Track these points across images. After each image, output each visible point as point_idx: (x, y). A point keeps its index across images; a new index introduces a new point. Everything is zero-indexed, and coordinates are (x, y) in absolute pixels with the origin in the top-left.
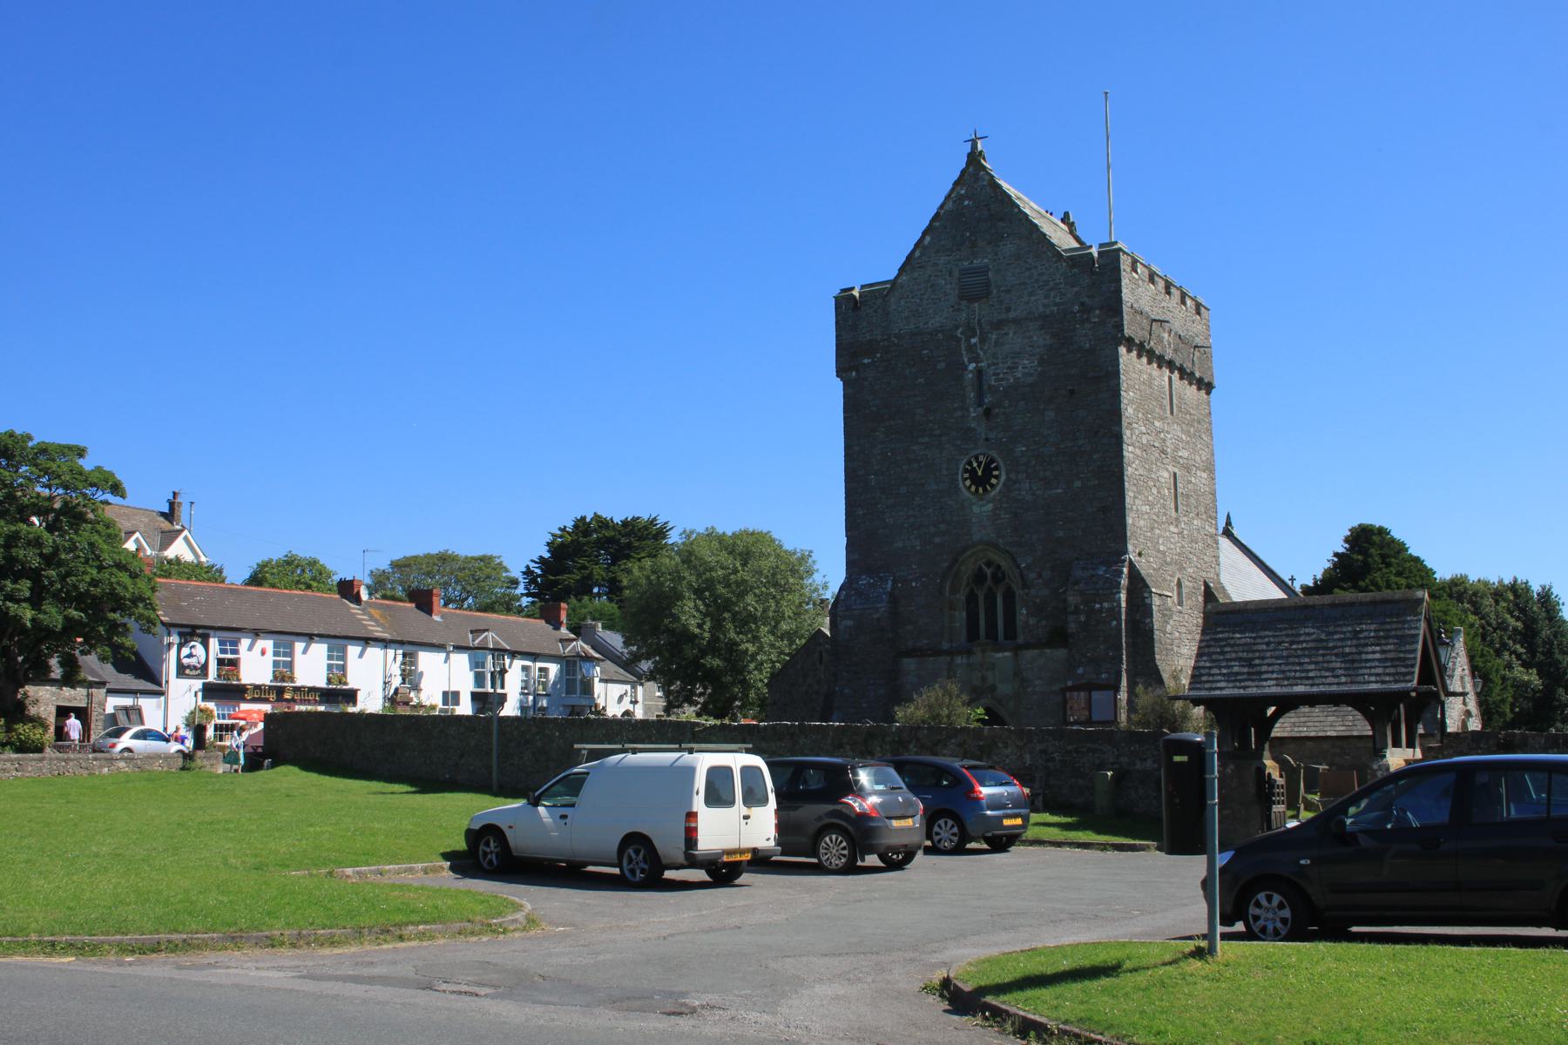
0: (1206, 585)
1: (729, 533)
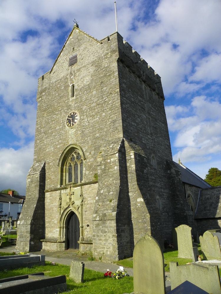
0: (167, 162)
1: (117, 245)
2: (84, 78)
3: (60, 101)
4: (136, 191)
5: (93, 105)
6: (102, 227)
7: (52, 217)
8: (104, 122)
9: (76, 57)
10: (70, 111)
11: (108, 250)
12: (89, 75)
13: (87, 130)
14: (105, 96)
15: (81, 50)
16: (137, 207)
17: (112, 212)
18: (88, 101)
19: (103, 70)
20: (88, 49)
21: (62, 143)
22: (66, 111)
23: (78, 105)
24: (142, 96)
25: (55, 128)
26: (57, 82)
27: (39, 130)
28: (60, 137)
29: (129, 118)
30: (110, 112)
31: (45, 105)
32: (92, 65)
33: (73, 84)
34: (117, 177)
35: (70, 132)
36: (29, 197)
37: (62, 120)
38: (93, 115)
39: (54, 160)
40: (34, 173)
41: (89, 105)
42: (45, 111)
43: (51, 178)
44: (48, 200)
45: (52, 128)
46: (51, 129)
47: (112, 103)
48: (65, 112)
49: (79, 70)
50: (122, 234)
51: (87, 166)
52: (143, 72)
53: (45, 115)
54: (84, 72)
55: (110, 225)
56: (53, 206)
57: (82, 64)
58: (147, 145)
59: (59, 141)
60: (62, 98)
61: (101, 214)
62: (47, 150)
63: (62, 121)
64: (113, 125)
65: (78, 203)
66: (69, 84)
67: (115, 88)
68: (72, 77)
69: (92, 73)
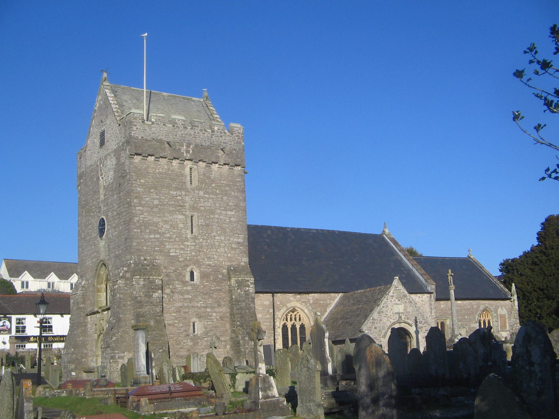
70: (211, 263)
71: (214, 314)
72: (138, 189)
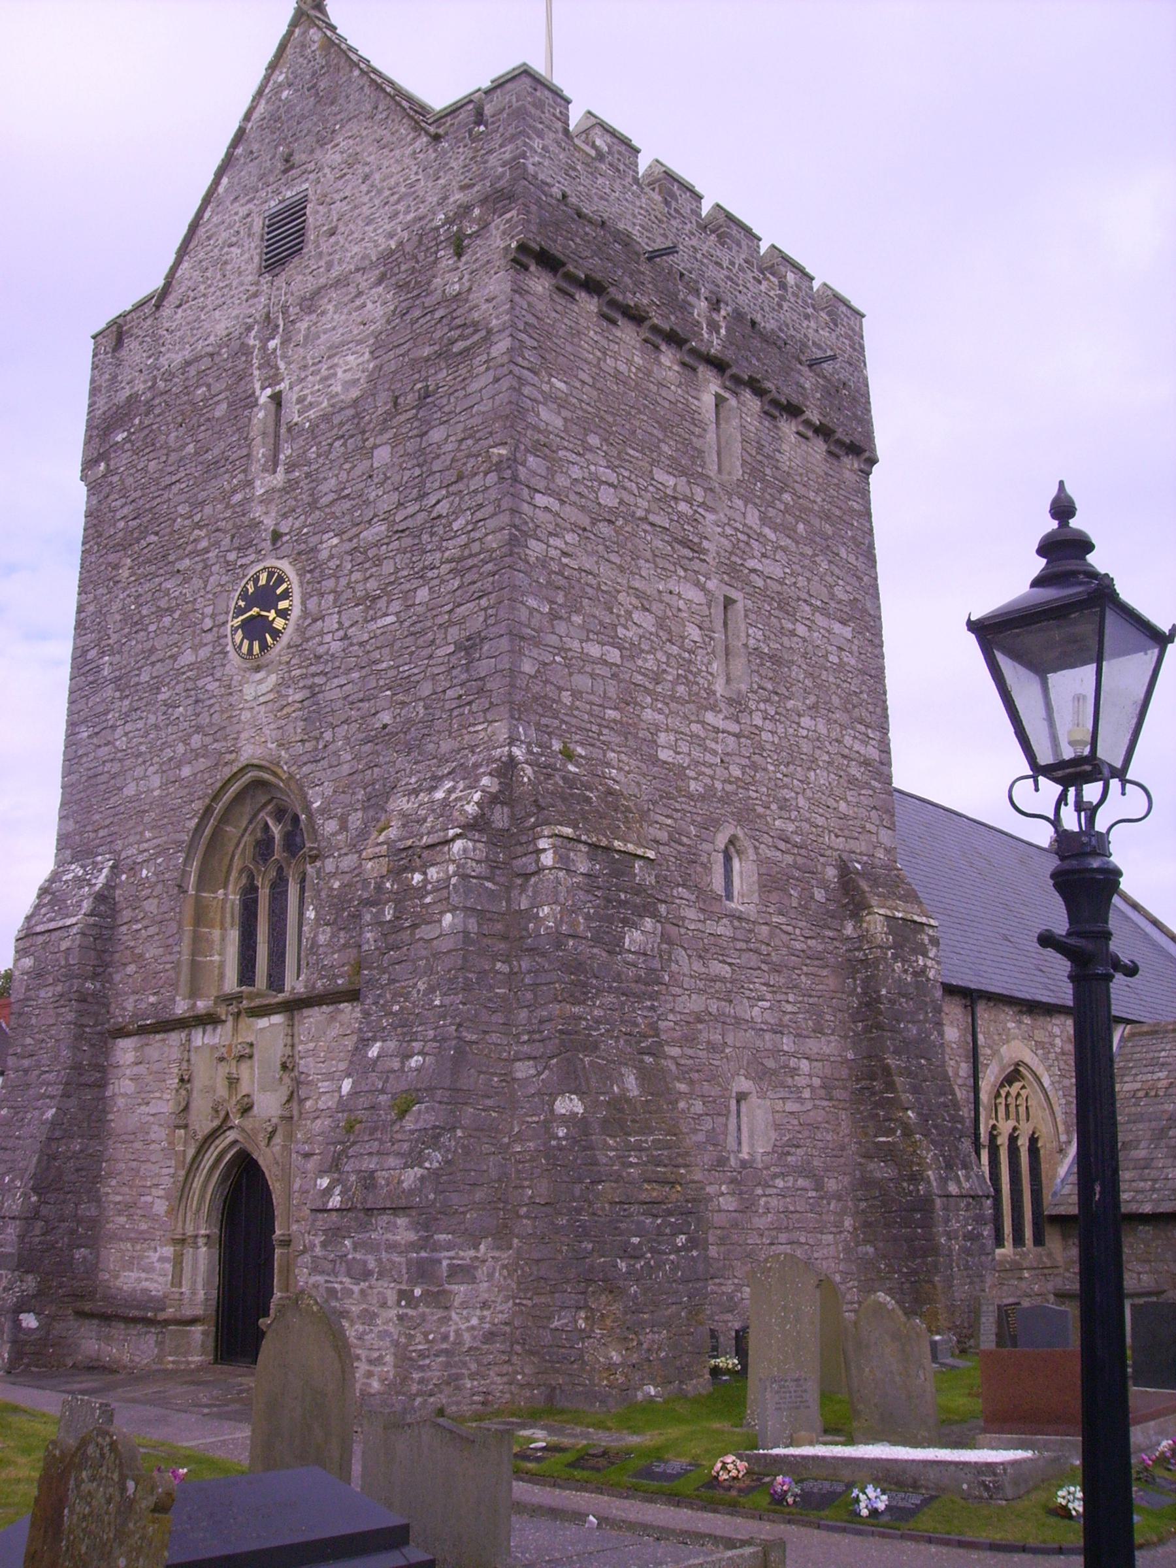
0: (844, 869)
2: (336, 360)
3: (204, 494)
4: (551, 1058)
5: (370, 535)
6: (355, 1249)
7: (144, 1178)
8: (420, 642)
9: (295, 213)
10: (253, 557)
11: (372, 1368)
12: (359, 342)
13: (336, 682)
14: (437, 484)
15: (327, 170)
16: (553, 1143)
17: (406, 1166)
18: (347, 504)
19: (438, 315)
20: (367, 169)
21: (203, 752)
22: (232, 556)
23: (297, 524)
24: (688, 465)
25: (174, 657)
26: (192, 371)
27: (92, 661)
28: (198, 715)
29: (569, 620)
30: (457, 583)
31: (125, 511)
32: (380, 281)
33: (278, 388)
34: (449, 971)
35: (249, 691)
36: (26, 1063)
37: (209, 610)
38: (367, 596)
39: (161, 851)
40: (52, 925)
41: (355, 530)
42: (123, 547)
43: (141, 955)
44: (128, 1082)
45: (160, 655)
46: (153, 664)
47: (470, 527)
48: (227, 563)
49: (309, 304)
50: (455, 1287)
51: (323, 894)
52: (716, 304)
53: (124, 573)
54: (335, 319)
55: (389, 1236)
56: (152, 1119)
57: (329, 266)
58: (692, 774)
59: (190, 736)
60: (215, 477)
61: (353, 1178)
62: (130, 790)
63: (213, 616)
64: (467, 668)
65: (268, 1105)
66: (257, 385)
67: (490, 441)
68: (272, 344)
69: (377, 327)
70: (791, 827)
71: (804, 1065)
72: (544, 413)
